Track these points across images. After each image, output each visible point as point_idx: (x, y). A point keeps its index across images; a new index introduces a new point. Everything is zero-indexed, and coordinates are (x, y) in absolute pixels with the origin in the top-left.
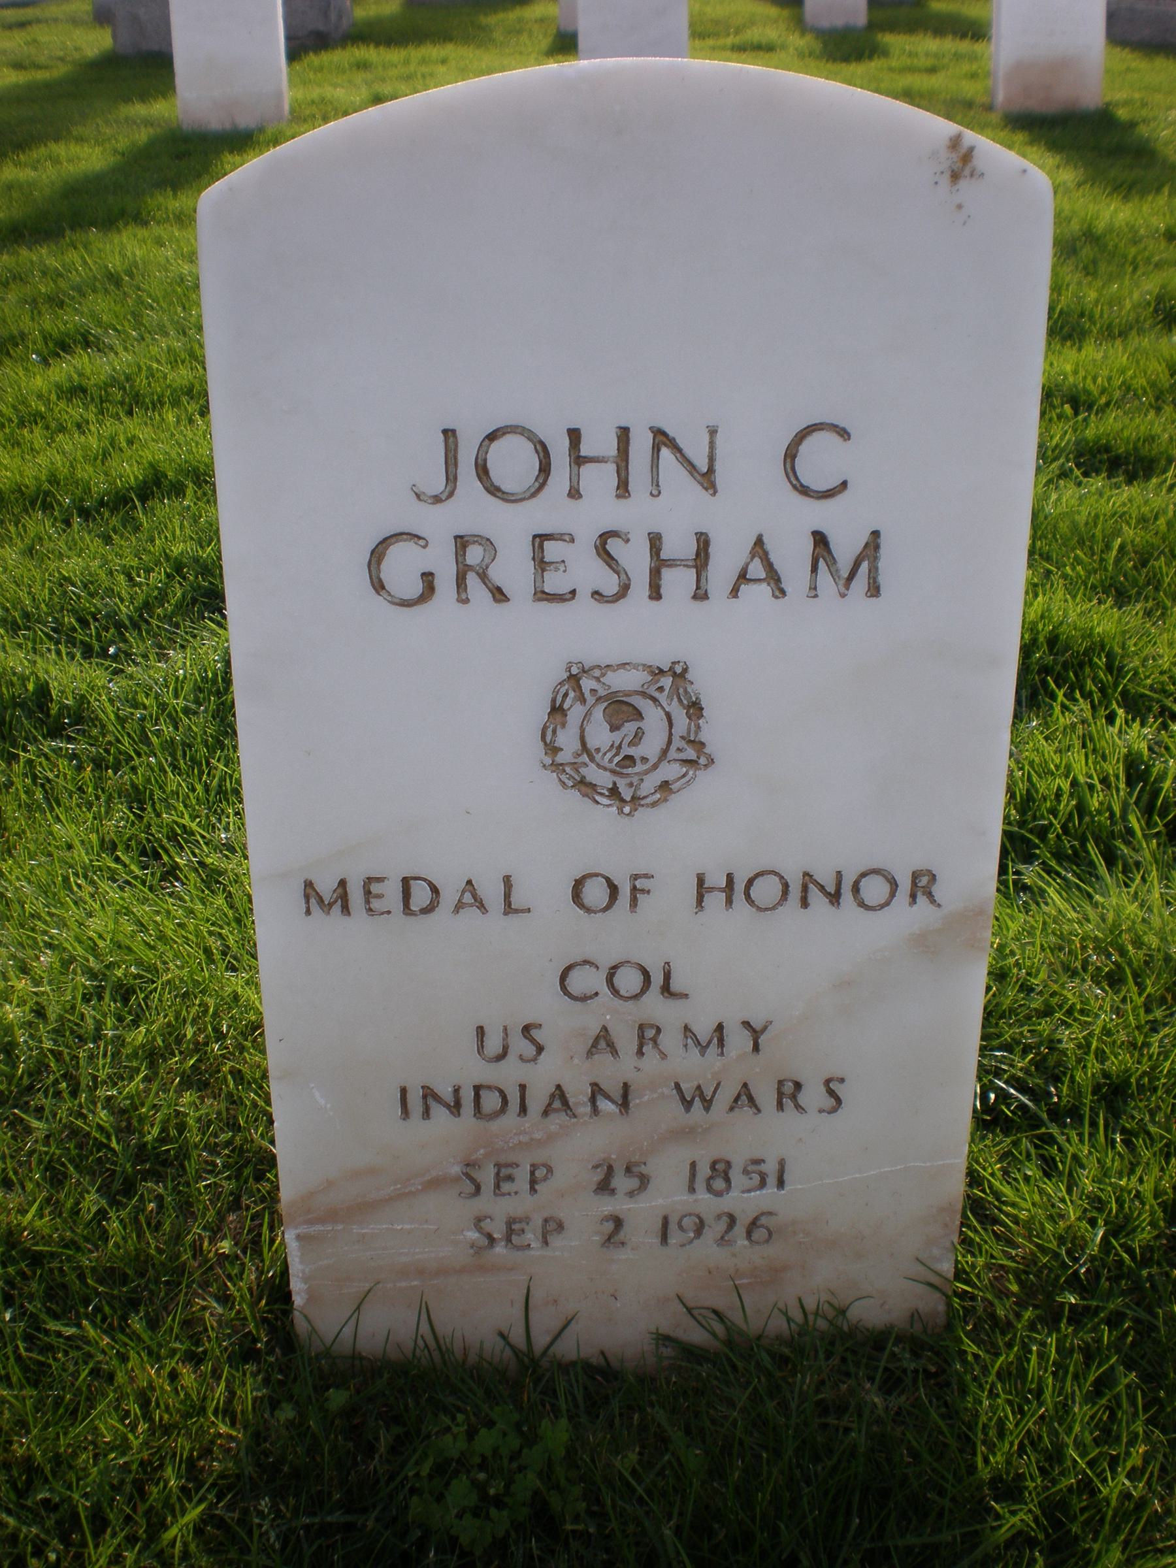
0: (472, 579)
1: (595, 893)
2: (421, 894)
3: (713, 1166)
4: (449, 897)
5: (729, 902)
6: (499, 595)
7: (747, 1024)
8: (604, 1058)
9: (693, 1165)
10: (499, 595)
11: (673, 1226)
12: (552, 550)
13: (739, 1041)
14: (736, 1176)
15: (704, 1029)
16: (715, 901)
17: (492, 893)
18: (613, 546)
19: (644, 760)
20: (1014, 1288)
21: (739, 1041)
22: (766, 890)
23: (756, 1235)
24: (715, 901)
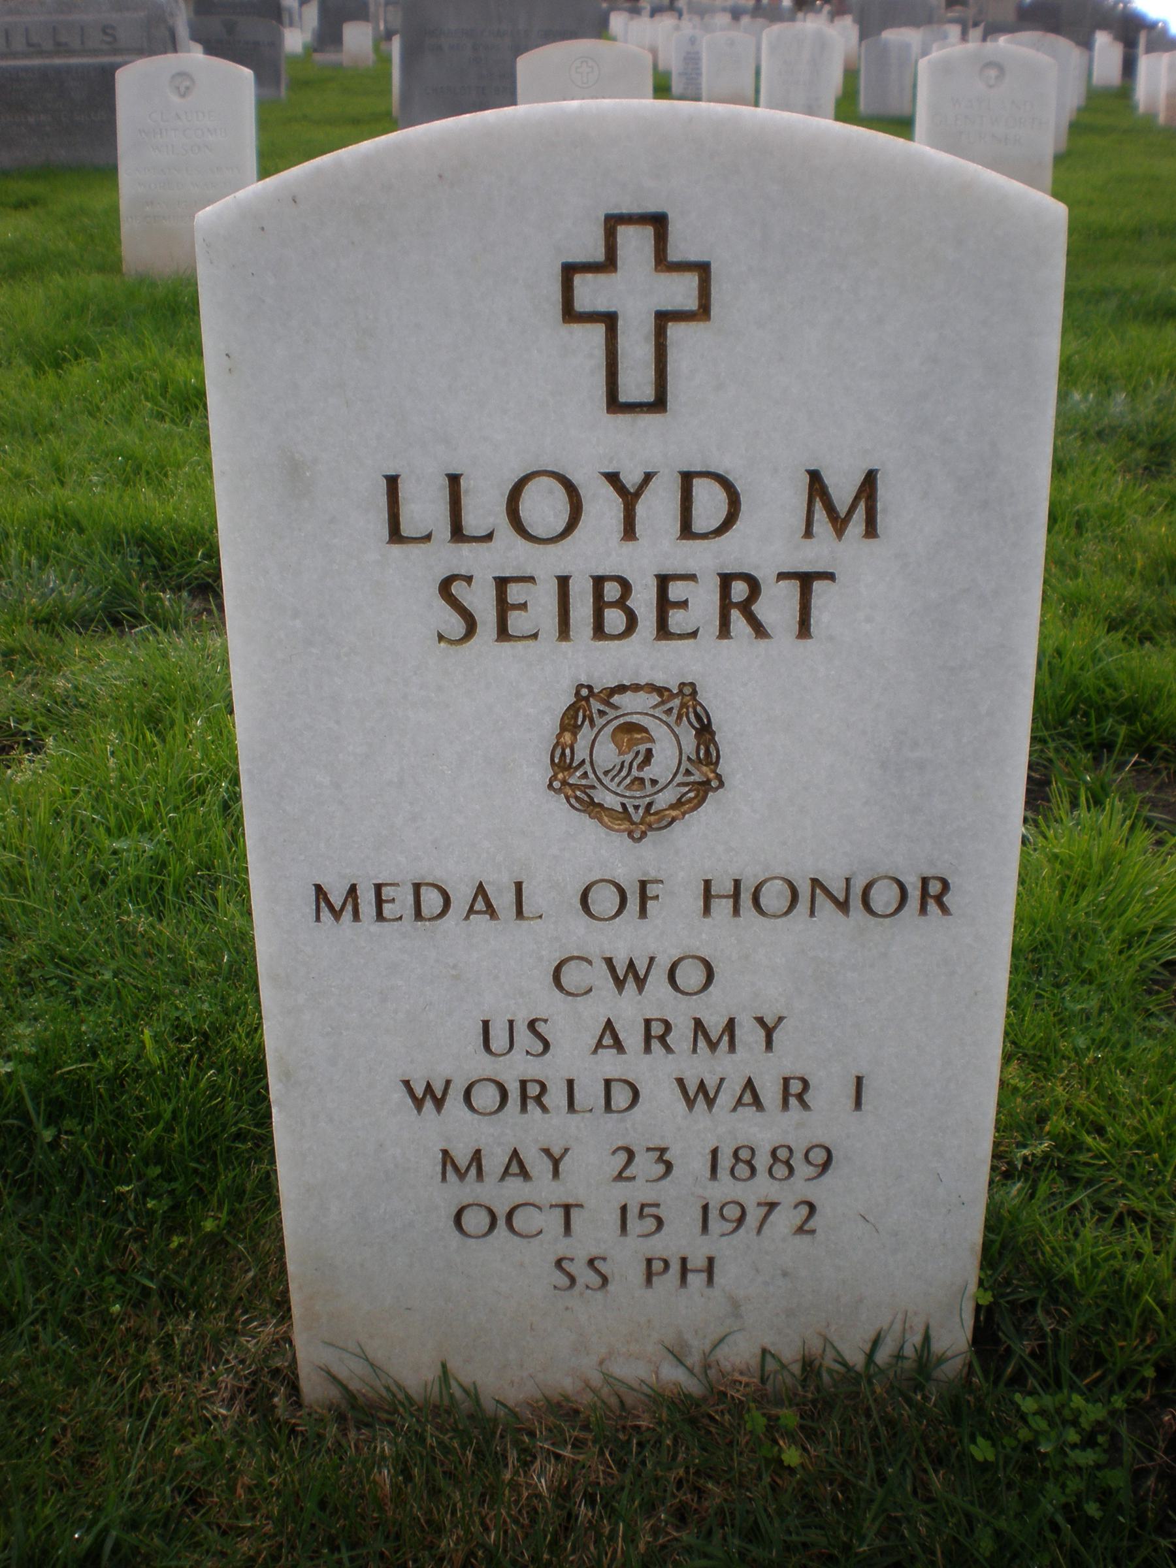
0: (735, 615)
1: (606, 899)
2: (432, 901)
3: (774, 1153)
4: (460, 903)
5: (736, 911)
6: (759, 630)
7: (760, 1021)
8: (608, 1055)
9: (715, 1153)
10: (759, 630)
11: (713, 1214)
12: (676, 591)
13: (751, 1035)
14: (797, 1162)
15: (715, 1024)
16: (723, 907)
17: (504, 901)
18: (457, 589)
19: (654, 782)
20: (174, 1244)
21: (751, 1035)
22: (884, 896)
23: (737, 1213)
24: (723, 907)
